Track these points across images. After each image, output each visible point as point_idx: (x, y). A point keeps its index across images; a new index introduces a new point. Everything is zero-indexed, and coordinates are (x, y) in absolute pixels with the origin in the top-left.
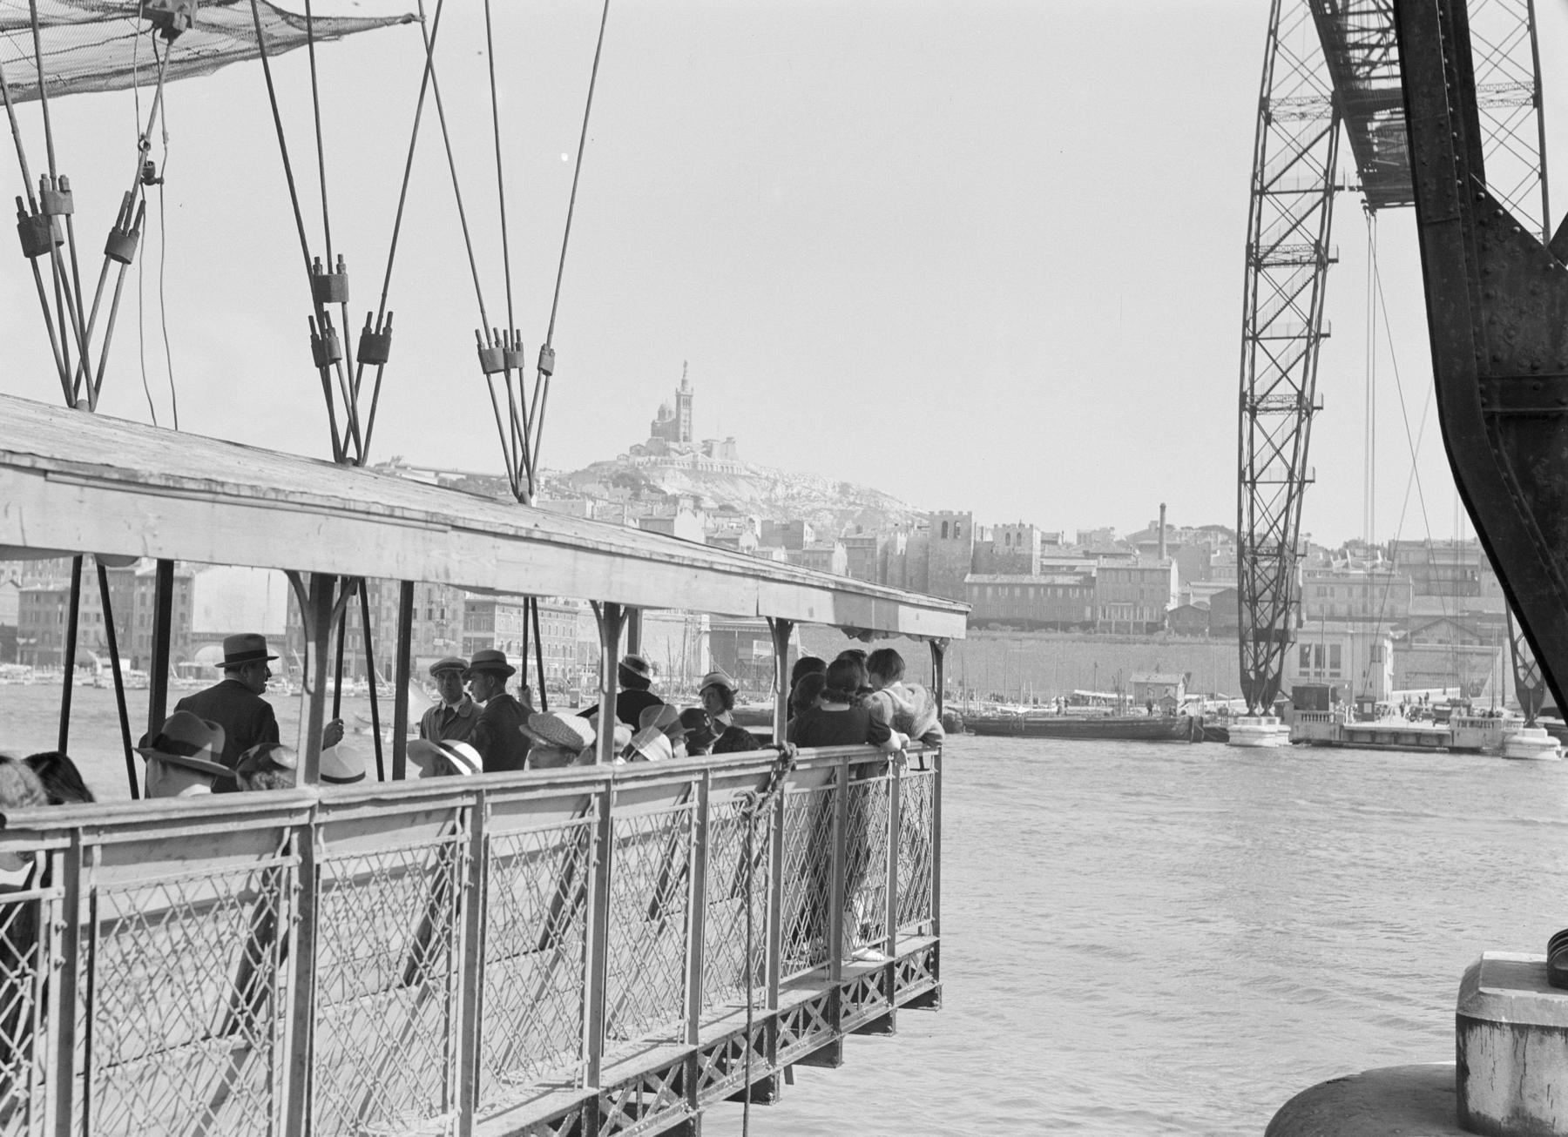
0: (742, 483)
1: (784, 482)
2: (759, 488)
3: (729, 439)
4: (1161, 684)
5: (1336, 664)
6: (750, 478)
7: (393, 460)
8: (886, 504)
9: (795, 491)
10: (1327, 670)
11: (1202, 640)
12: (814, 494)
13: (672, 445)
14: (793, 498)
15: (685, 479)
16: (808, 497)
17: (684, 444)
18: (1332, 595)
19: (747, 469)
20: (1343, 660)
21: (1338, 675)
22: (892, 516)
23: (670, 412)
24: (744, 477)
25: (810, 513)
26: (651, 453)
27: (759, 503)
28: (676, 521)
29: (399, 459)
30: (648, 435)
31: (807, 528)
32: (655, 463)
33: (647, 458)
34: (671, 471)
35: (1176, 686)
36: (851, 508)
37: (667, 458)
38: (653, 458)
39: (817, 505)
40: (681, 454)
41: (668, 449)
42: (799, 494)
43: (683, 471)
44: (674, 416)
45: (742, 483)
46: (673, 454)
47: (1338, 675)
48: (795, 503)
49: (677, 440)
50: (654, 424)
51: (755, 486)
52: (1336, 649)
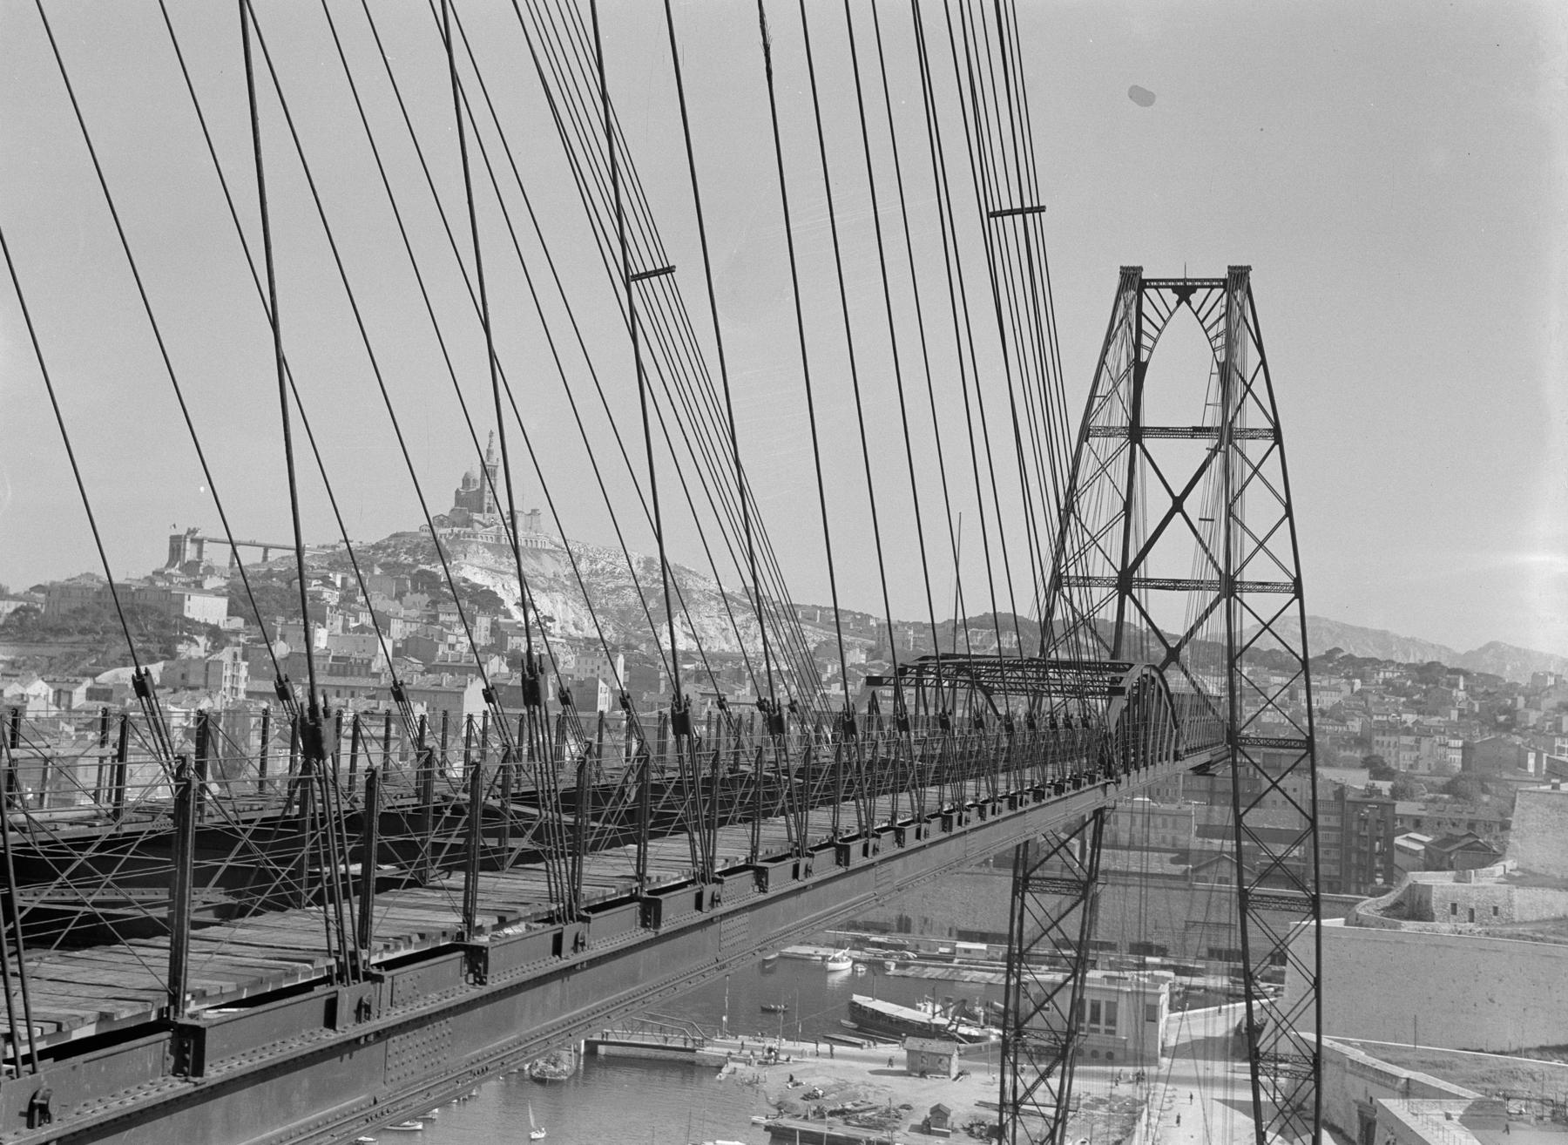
0: (545, 557)
1: (588, 557)
2: (563, 563)
3: (534, 511)
4: (937, 1055)
5: (1112, 1021)
6: (554, 552)
7: (188, 533)
8: (690, 583)
9: (599, 566)
10: (1102, 1026)
11: (987, 871)
12: (618, 570)
13: (477, 516)
14: (596, 574)
15: (488, 555)
16: (612, 573)
17: (488, 516)
18: (1116, 823)
19: (551, 543)
20: (1118, 1019)
21: (1113, 1032)
22: (695, 596)
23: (475, 481)
24: (548, 551)
25: (614, 591)
26: (455, 524)
27: (563, 579)
28: (466, 693)
29: (195, 531)
30: (451, 503)
31: (601, 684)
32: (457, 535)
33: (449, 530)
34: (474, 547)
35: (950, 1057)
36: (655, 586)
37: (469, 530)
38: (456, 530)
39: (621, 582)
40: (485, 526)
41: (472, 520)
42: (603, 569)
43: (486, 545)
44: (478, 487)
45: (545, 557)
46: (477, 526)
47: (1113, 1032)
48: (599, 580)
49: (481, 511)
50: (457, 492)
51: (559, 562)
52: (1112, 1006)
